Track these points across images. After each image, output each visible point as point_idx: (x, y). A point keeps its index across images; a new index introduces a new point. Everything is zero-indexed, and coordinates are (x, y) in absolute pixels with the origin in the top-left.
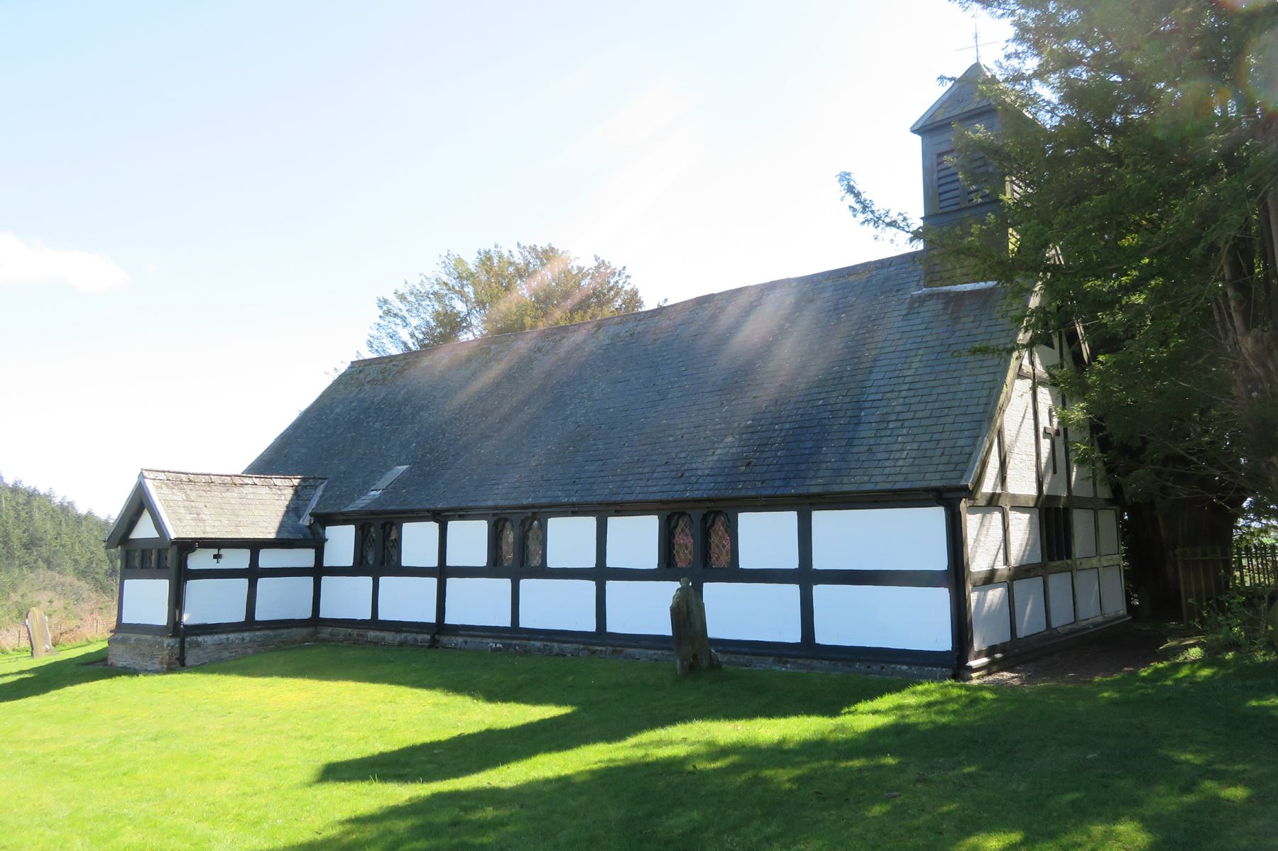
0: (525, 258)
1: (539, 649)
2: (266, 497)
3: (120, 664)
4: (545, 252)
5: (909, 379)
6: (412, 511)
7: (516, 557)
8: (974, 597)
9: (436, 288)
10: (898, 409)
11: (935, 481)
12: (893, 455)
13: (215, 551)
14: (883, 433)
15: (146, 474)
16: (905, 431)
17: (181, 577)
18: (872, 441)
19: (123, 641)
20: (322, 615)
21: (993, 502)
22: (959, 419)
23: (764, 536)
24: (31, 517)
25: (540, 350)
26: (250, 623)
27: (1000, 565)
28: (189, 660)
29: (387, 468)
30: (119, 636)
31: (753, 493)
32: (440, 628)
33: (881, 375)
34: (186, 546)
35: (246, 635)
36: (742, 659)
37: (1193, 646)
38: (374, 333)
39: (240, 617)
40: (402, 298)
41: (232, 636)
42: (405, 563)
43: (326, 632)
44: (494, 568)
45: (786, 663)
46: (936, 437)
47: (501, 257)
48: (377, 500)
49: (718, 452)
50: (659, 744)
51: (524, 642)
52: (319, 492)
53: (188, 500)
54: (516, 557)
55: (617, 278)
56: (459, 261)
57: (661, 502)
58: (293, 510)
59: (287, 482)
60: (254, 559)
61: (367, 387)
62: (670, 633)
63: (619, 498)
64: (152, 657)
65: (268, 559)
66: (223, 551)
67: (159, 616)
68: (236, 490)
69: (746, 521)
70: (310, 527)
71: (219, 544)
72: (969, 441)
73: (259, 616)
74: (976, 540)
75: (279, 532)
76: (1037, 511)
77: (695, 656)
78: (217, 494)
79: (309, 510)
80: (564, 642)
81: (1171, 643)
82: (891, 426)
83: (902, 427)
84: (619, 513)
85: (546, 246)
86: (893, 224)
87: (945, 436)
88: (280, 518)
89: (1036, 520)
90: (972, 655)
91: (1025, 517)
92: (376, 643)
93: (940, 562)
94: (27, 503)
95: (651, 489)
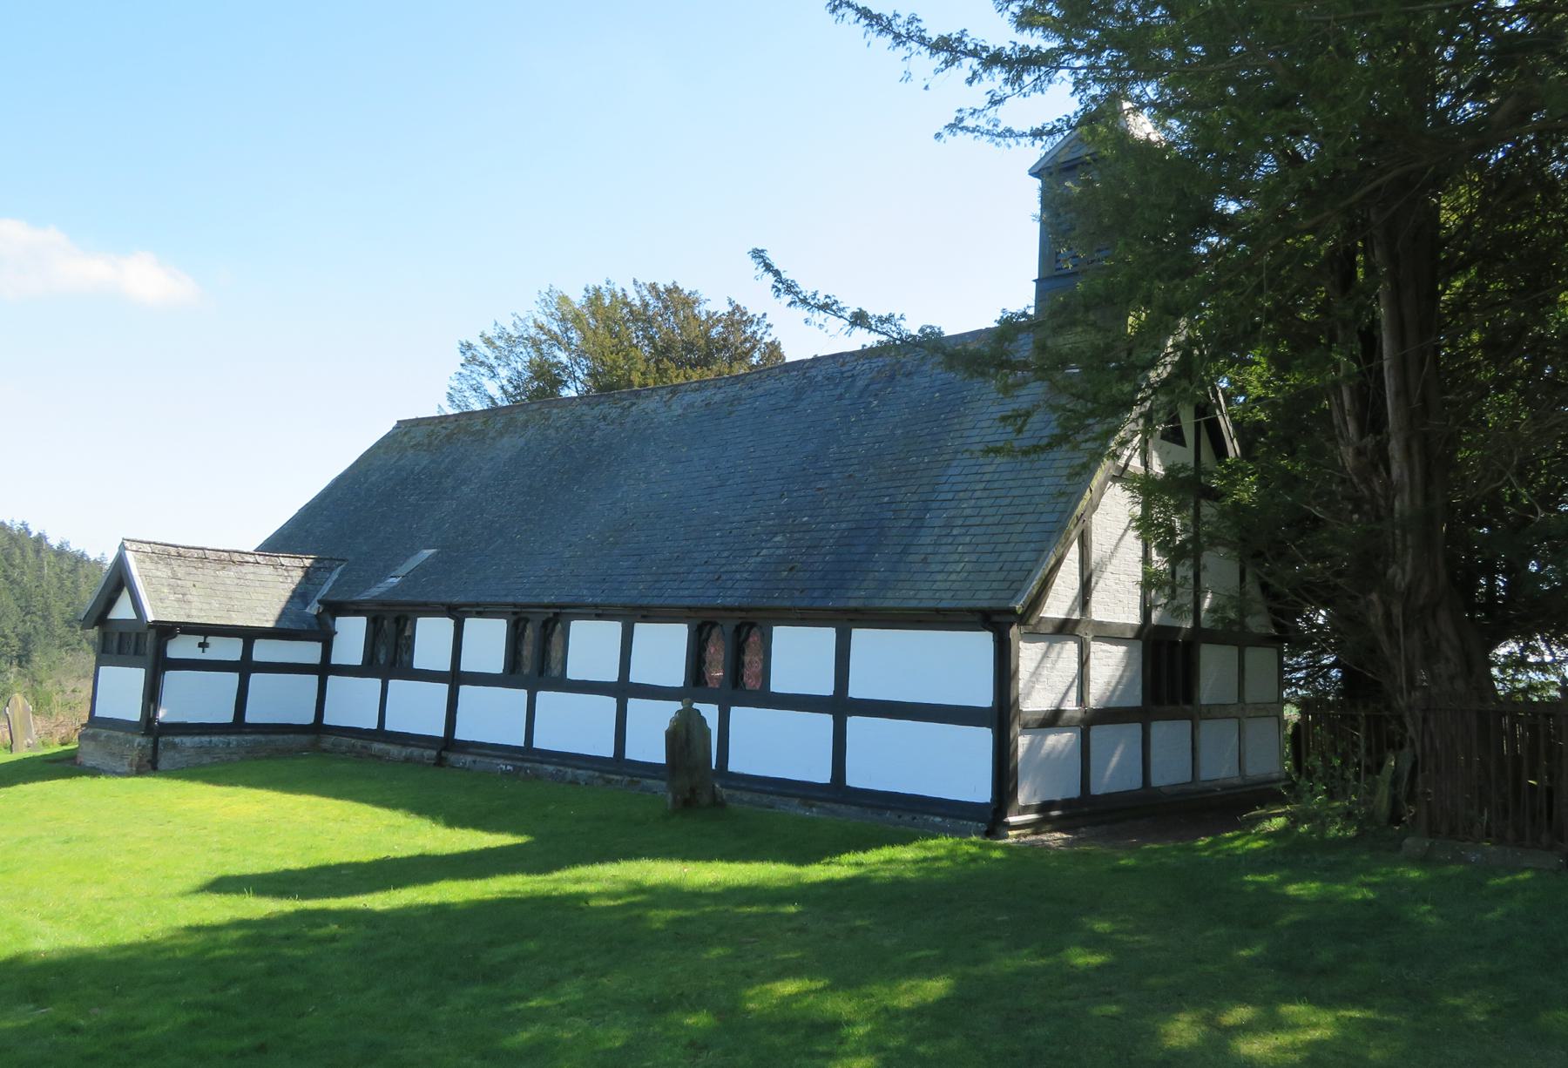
0: (642, 299)
1: (552, 775)
2: (270, 578)
3: (89, 764)
4: (668, 291)
5: (987, 477)
6: (425, 604)
7: (535, 665)
8: (1023, 742)
9: (533, 331)
10: (968, 512)
11: (983, 601)
12: (950, 568)
13: (201, 639)
14: (944, 540)
15: (127, 544)
16: (968, 539)
17: (158, 667)
18: (930, 550)
19: (94, 737)
20: (326, 721)
21: (1064, 629)
22: (1029, 529)
23: (799, 656)
24: (77, 587)
25: (604, 418)
26: (239, 724)
27: (1071, 705)
28: (163, 763)
29: (414, 551)
30: (90, 731)
31: (787, 604)
32: (448, 744)
33: (957, 471)
34: (166, 631)
35: (233, 739)
36: (766, 799)
37: (1279, 815)
38: (455, 384)
39: (228, 718)
40: (489, 342)
41: (215, 739)
42: (417, 665)
43: (328, 741)
44: (512, 675)
45: (811, 806)
46: (1000, 548)
47: (614, 295)
48: (394, 589)
49: (764, 552)
50: (578, 881)
51: (537, 765)
52: (335, 576)
53: (175, 577)
54: (535, 665)
55: (754, 328)
56: (564, 299)
57: (689, 608)
58: (300, 596)
59: (297, 562)
60: (247, 650)
61: (410, 453)
62: (662, 760)
63: (645, 602)
64: (122, 757)
65: (263, 651)
66: (210, 639)
67: (132, 711)
68: (234, 568)
69: (782, 636)
70: (317, 616)
71: (206, 631)
72: (1033, 556)
73: (250, 718)
74: (1035, 673)
75: (278, 621)
76: (1139, 643)
77: (693, 791)
78: (209, 570)
79: (319, 597)
80: (579, 768)
81: (1260, 812)
82: (955, 532)
83: (965, 534)
84: (646, 619)
85: (669, 284)
86: (824, 307)
87: (1010, 547)
88: (282, 604)
89: (1138, 655)
90: (1013, 808)
91: (1119, 651)
92: (380, 758)
93: (983, 697)
94: (73, 571)
95: (682, 593)
